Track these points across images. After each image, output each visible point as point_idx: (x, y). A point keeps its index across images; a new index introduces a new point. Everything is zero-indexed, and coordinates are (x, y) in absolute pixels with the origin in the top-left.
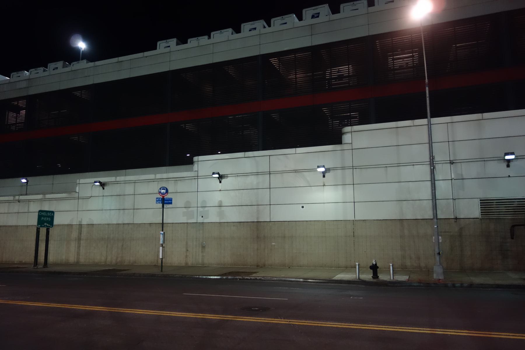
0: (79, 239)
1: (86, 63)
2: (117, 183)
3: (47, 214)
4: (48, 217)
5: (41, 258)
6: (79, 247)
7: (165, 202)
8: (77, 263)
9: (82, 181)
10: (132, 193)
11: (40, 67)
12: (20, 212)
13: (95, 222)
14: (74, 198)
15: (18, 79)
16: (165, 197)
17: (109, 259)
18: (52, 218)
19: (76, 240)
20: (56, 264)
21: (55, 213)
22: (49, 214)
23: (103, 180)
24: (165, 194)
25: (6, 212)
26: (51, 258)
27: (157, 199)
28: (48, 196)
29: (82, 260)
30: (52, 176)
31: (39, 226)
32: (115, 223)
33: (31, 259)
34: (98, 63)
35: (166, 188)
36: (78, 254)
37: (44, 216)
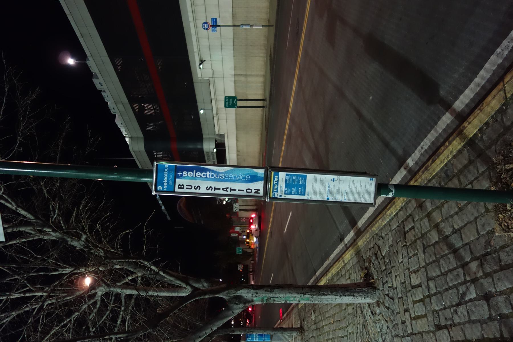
0: (246, 76)
1: (89, 61)
2: (199, 51)
3: (227, 102)
4: (229, 100)
6: (251, 75)
7: (215, 24)
8: (265, 76)
9: (199, 75)
10: (207, 40)
12: (225, 113)
13: (233, 66)
14: (214, 80)
15: (116, 108)
16: (211, 25)
17: (262, 55)
18: (230, 97)
20: (264, 95)
21: (226, 96)
22: (227, 100)
23: (198, 62)
24: (208, 25)
27: (213, 31)
28: (213, 97)
29: (262, 73)
31: (236, 107)
32: (232, 52)
34: (88, 53)
35: (203, 23)
36: (257, 76)
37: (229, 103)
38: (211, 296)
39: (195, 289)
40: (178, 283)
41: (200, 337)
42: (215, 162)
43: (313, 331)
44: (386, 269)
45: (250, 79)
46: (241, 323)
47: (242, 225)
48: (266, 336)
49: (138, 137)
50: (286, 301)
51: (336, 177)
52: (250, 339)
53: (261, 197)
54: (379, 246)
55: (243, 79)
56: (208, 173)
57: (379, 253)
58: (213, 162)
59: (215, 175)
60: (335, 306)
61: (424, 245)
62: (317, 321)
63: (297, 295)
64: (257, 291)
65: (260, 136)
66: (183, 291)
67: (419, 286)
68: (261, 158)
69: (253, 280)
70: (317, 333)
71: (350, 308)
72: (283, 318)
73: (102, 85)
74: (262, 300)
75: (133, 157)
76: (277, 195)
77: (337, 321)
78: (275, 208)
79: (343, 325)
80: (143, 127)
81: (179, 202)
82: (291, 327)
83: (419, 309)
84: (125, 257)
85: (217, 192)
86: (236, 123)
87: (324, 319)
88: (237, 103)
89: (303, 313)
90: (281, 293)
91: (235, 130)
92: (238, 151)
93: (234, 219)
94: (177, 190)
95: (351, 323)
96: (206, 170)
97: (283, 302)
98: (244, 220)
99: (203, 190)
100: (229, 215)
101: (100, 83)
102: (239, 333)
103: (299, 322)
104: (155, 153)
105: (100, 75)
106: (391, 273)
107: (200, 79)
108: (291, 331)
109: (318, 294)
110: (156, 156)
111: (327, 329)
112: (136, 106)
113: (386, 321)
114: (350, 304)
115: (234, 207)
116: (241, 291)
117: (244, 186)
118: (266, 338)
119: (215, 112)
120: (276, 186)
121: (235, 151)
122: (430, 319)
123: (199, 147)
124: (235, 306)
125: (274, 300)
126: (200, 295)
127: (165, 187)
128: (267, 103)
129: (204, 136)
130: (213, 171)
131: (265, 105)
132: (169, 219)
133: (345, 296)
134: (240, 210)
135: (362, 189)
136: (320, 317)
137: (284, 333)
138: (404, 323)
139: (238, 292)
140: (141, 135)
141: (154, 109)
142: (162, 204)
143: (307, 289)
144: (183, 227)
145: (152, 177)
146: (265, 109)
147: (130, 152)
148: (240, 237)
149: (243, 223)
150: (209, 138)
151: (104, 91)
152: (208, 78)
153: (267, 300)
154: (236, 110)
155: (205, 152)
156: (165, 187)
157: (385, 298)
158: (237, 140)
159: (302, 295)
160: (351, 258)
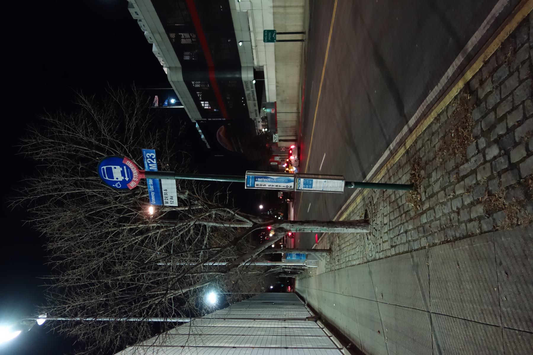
0: (285, 7)
3: (266, 36)
4: (268, 34)
5: (299, 37)
6: (291, 7)
8: (304, 7)
9: (238, 8)
11: (138, 25)
14: (252, 13)
15: (152, 37)
19: (285, 9)
20: (304, 26)
21: (265, 29)
25: (265, 53)
26: (299, 29)
29: (302, 4)
30: (231, 10)
31: (275, 41)
33: (299, 43)
36: (296, 7)
38: (264, 228)
39: (255, 224)
40: (245, 220)
41: (258, 252)
42: (253, 91)
43: (337, 251)
44: (374, 213)
45: (289, 10)
46: (281, 247)
47: (281, 154)
48: (302, 256)
49: (176, 67)
50: (312, 231)
51: (326, 180)
52: (290, 257)
53: (292, 189)
54: (373, 197)
55: (281, 10)
56: (269, 179)
57: (372, 202)
58: (252, 91)
59: (272, 180)
60: (350, 234)
61: (390, 201)
62: (340, 244)
63: (318, 227)
64: (293, 224)
65: (299, 67)
66: (246, 224)
67: (386, 224)
68: (300, 88)
69: (293, 207)
70: (340, 253)
71: (358, 235)
72: (318, 242)
73: (138, 14)
74: (296, 230)
75: (172, 87)
76: (300, 188)
77: (351, 244)
78: (312, 146)
79: (354, 247)
80: (180, 56)
81: (218, 131)
82: (323, 248)
83: (386, 238)
84: (218, 207)
85: (273, 187)
86: (275, 55)
87: (345, 243)
88: (276, 37)
89: (332, 238)
90: (309, 226)
91: (274, 61)
92: (277, 82)
93: (274, 148)
94: (256, 186)
95: (358, 245)
96: (268, 178)
97: (310, 232)
98: (284, 149)
99: (267, 186)
100: (269, 145)
101: (136, 12)
102: (280, 253)
103: (329, 245)
104: (193, 83)
105: (136, 5)
106: (377, 215)
107: (239, 12)
108: (322, 251)
109: (332, 227)
110: (195, 85)
111: (345, 249)
112: (173, 35)
113: (373, 244)
114: (358, 233)
115: (274, 138)
116: (283, 225)
117: (285, 185)
118: (302, 257)
119: (253, 44)
120: (299, 184)
121: (275, 83)
122: (389, 242)
123: (237, 76)
124: (279, 234)
125: (304, 230)
126: (258, 227)
127: (250, 185)
128: (306, 37)
129: (242, 65)
130: (271, 178)
131: (304, 38)
132: (209, 147)
133: (350, 228)
134: (280, 140)
135: (339, 186)
136: (342, 241)
137: (316, 253)
138: (380, 244)
139: (281, 225)
140: (179, 65)
141: (191, 38)
142: (201, 133)
143: (325, 224)
144: (223, 156)
145: (245, 180)
146: (304, 42)
147: (169, 82)
148: (280, 166)
149: (283, 152)
150: (248, 67)
151: (140, 21)
152: (246, 11)
153: (300, 230)
154: (275, 46)
155: (243, 82)
156: (250, 185)
157: (373, 230)
158: (276, 72)
159: (322, 227)
160: (360, 202)
